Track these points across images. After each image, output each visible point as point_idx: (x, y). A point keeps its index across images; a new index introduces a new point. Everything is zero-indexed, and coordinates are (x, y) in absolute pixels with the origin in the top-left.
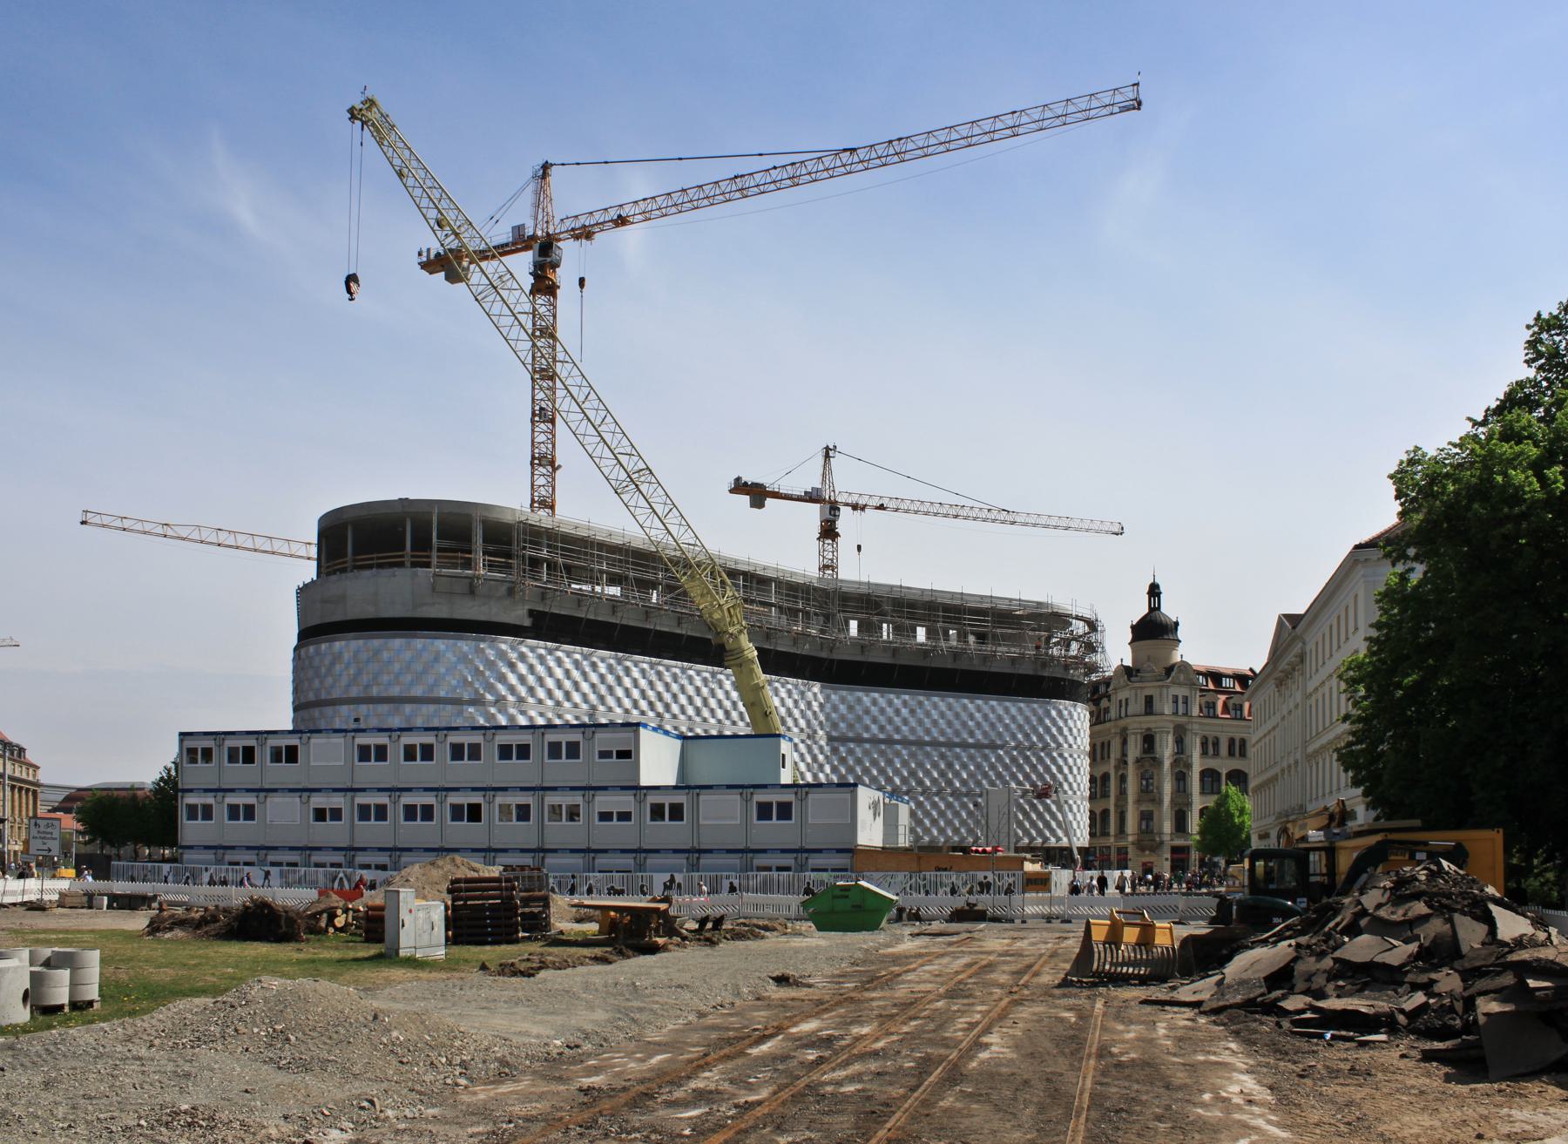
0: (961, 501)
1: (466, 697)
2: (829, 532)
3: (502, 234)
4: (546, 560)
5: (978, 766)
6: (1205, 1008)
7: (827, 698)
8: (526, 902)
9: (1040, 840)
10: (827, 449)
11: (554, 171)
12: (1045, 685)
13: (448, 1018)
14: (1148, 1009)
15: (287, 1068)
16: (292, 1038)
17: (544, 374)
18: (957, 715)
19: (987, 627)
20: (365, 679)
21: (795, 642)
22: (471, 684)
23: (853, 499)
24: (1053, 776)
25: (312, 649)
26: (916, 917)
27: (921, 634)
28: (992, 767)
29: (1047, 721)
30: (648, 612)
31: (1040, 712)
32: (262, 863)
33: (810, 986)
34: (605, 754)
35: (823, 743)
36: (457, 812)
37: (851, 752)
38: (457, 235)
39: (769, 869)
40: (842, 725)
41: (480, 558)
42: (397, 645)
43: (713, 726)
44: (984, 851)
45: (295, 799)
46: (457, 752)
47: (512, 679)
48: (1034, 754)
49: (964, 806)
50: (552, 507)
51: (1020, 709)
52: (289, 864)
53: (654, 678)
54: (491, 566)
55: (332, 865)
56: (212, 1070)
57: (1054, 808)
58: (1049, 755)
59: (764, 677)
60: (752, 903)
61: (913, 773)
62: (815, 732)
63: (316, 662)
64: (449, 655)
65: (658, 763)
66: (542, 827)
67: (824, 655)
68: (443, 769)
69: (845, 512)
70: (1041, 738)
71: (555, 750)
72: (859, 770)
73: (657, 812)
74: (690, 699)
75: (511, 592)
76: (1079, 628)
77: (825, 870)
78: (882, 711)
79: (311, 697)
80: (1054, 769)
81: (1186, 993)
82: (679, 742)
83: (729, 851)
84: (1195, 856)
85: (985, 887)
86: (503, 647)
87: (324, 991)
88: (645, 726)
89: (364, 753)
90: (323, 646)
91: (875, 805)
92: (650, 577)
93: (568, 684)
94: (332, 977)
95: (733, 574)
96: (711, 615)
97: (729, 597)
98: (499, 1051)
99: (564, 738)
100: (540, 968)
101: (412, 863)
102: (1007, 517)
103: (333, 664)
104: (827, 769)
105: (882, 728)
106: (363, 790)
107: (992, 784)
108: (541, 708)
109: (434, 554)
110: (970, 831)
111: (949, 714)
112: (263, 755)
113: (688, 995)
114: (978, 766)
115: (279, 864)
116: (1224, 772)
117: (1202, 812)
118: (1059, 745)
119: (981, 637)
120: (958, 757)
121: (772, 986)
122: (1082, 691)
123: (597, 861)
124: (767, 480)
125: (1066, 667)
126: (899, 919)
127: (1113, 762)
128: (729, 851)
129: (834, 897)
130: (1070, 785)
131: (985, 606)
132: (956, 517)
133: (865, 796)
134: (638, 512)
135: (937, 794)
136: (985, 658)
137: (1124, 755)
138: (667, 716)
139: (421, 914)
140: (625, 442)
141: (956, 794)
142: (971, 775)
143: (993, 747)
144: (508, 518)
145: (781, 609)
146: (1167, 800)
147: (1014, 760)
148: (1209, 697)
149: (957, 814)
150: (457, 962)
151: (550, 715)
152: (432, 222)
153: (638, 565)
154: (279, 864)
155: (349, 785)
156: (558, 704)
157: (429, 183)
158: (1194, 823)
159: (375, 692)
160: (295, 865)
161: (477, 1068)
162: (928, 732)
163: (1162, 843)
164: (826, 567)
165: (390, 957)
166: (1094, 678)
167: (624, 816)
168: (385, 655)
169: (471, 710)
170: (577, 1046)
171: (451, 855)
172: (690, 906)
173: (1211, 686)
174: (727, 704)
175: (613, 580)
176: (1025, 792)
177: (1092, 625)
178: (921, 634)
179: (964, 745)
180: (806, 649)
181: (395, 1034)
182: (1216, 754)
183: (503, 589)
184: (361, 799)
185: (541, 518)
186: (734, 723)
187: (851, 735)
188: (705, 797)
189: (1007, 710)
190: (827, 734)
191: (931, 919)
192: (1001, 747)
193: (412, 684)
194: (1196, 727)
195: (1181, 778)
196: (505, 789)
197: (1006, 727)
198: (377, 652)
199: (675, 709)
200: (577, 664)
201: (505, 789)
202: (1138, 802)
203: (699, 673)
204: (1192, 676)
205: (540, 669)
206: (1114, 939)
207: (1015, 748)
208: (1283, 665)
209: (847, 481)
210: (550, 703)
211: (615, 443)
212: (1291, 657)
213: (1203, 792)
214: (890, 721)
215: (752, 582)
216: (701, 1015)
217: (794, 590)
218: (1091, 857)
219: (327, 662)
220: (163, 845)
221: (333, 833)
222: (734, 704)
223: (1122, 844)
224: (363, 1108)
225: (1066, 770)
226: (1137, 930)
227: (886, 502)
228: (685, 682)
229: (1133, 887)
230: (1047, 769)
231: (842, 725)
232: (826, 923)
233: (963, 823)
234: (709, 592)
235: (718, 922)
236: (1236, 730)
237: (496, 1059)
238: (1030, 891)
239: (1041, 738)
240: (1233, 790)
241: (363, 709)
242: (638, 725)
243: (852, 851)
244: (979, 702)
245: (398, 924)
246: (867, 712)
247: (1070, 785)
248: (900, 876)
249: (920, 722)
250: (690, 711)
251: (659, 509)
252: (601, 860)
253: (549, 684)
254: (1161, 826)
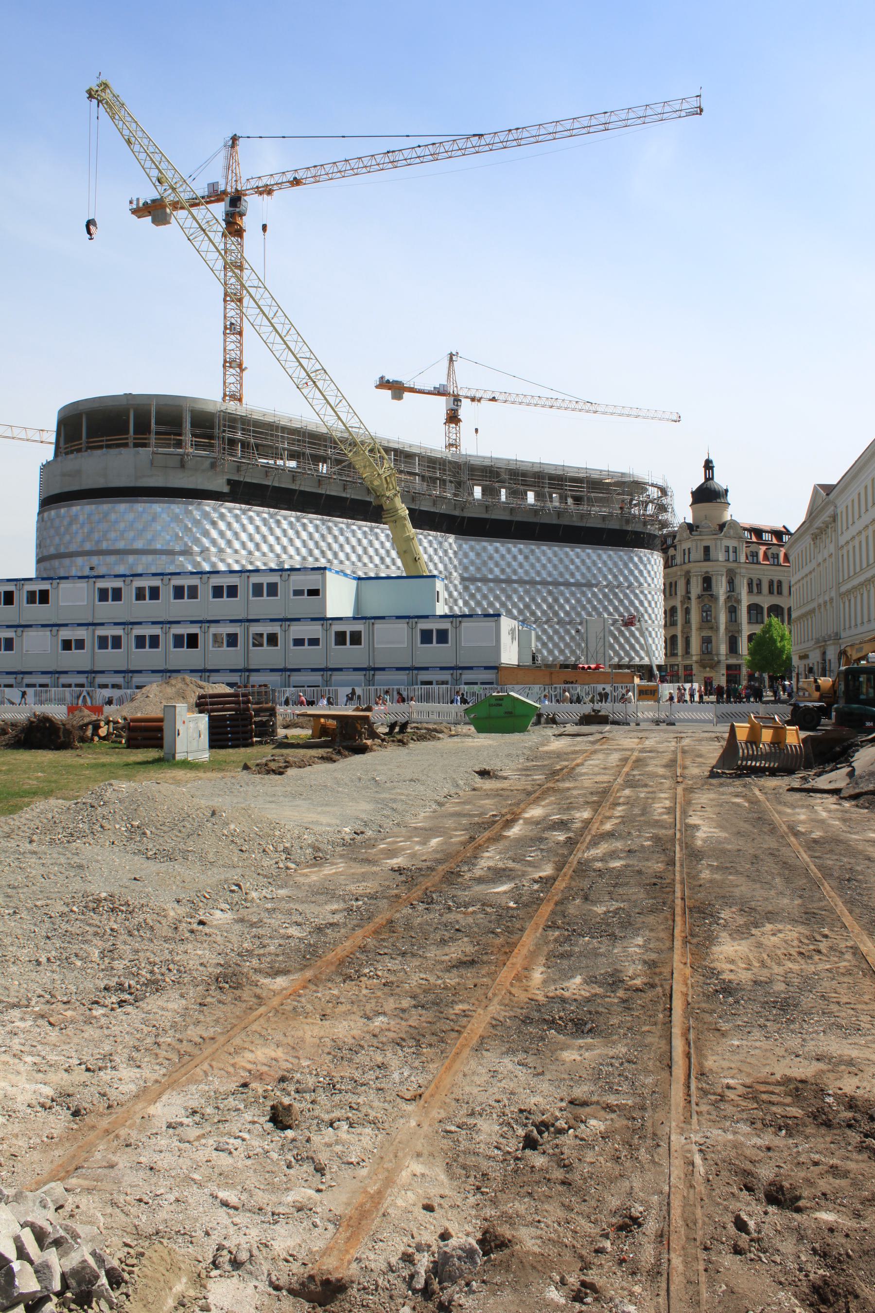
0: (554, 395)
1: (177, 549)
2: (453, 418)
3: (201, 189)
4: (240, 441)
5: (578, 601)
6: (844, 794)
7: (460, 547)
8: (258, 712)
9: (627, 659)
10: (451, 355)
11: (241, 142)
12: (627, 536)
13: (273, 813)
14: (798, 795)
15: (155, 857)
16: (148, 832)
17: (234, 297)
18: (561, 561)
19: (584, 492)
20: (96, 536)
21: (434, 503)
22: (181, 538)
23: (471, 394)
24: (636, 609)
25: (53, 513)
26: (553, 721)
27: (531, 497)
28: (589, 601)
29: (631, 565)
30: (320, 480)
31: (625, 558)
32: (19, 685)
33: (506, 778)
34: (298, 593)
35: (457, 582)
36: (178, 641)
37: (478, 589)
38: (174, 189)
39: (430, 683)
40: (471, 568)
41: (187, 437)
42: (122, 509)
43: (371, 569)
44: (589, 668)
45: (47, 633)
46: (179, 592)
47: (214, 534)
48: (621, 591)
49: (568, 632)
50: (240, 400)
51: (610, 556)
52: (41, 686)
53: (325, 532)
54: (197, 446)
55: (77, 685)
56: (97, 861)
57: (637, 634)
58: (633, 592)
59: (413, 530)
60: (418, 711)
61: (527, 606)
62: (451, 574)
63: (57, 523)
64: (164, 516)
65: (339, 600)
66: (247, 652)
67: (457, 513)
68: (168, 606)
69: (465, 403)
70: (626, 578)
71: (258, 590)
72: (485, 603)
73: (340, 638)
74: (353, 548)
75: (213, 466)
76: (654, 493)
77: (476, 683)
78: (503, 557)
79: (52, 551)
80: (637, 603)
81: (822, 782)
82: (355, 582)
83: (398, 669)
84: (744, 671)
85: (604, 697)
86: (207, 509)
87: (135, 788)
88: (330, 570)
89: (103, 595)
90: (63, 511)
91: (512, 631)
92: (321, 453)
93: (258, 538)
94: (129, 778)
95: (387, 450)
96: (372, 482)
97: (388, 465)
98: (309, 838)
99: (265, 580)
100: (286, 767)
101: (151, 683)
102: (591, 407)
103: (70, 524)
104: (461, 603)
105: (503, 571)
106: (102, 624)
107: (589, 614)
108: (237, 557)
109: (153, 436)
110: (573, 652)
111: (555, 560)
112: (21, 598)
113: (422, 788)
114: (578, 601)
115: (70, 686)
116: (766, 606)
117: (750, 638)
118: (641, 585)
119: (578, 500)
120: (562, 594)
121: (478, 779)
122: (658, 542)
123: (292, 678)
124: (406, 379)
125: (645, 524)
126: (538, 723)
127: (679, 598)
128: (398, 669)
129: (491, 705)
130: (650, 615)
131: (581, 475)
132: (551, 407)
133: (507, 624)
134: (315, 402)
135: (546, 622)
136: (582, 516)
137: (688, 592)
138: (335, 562)
139: (192, 725)
140: (305, 348)
141: (560, 622)
142: (573, 608)
143: (589, 585)
144: (210, 408)
145: (423, 478)
146: (722, 628)
147: (606, 596)
148: (753, 548)
149: (562, 638)
150: (220, 763)
151: (244, 562)
152: (154, 180)
153: (311, 444)
154: (34, 686)
155: (90, 620)
156: (250, 553)
157: (151, 149)
158: (744, 647)
159: (104, 546)
160: (46, 686)
161: (297, 853)
162: (538, 573)
163: (719, 662)
164: (451, 445)
165: (168, 761)
166: (665, 531)
167: (314, 642)
168: (113, 517)
169: (181, 559)
170: (362, 833)
171: (180, 676)
172: (382, 715)
173: (754, 539)
174: (382, 552)
175: (293, 456)
176: (615, 621)
177: (664, 491)
178: (531, 497)
179: (567, 584)
180: (443, 509)
181: (232, 826)
182: (760, 592)
183: (207, 463)
184: (101, 632)
185: (232, 407)
186: (388, 567)
187: (478, 576)
188: (379, 626)
189: (599, 556)
190: (460, 575)
191: (564, 723)
192: (596, 586)
193: (134, 539)
194: (743, 571)
195: (733, 611)
196: (217, 622)
197: (599, 569)
198: (106, 515)
199: (342, 556)
200: (265, 521)
201: (217, 622)
202: (700, 629)
203: (360, 528)
204: (741, 531)
205: (236, 526)
206: (754, 739)
207: (606, 586)
208: (819, 523)
209: (466, 381)
210: (244, 552)
211: (298, 349)
212: (825, 517)
213: (749, 623)
214: (509, 565)
215: (402, 456)
216: (440, 804)
217: (432, 462)
218: (668, 673)
219: (65, 523)
221: (77, 659)
222: (388, 552)
223: (688, 662)
224: (232, 891)
225: (646, 604)
226: (771, 731)
227: (497, 396)
228: (349, 535)
229: (701, 697)
230: (632, 603)
231: (471, 568)
232: (485, 725)
233: (567, 645)
234: (371, 465)
235: (404, 726)
236: (776, 574)
237: (309, 845)
238: (643, 700)
239: (626, 578)
240: (775, 620)
241: (95, 560)
242: (325, 569)
243: (496, 668)
244: (578, 550)
245: (176, 733)
246: (491, 558)
247: (650, 615)
248: (536, 688)
249: (533, 566)
250: (354, 558)
251: (332, 401)
252: (296, 678)
253: (244, 539)
254: (718, 649)
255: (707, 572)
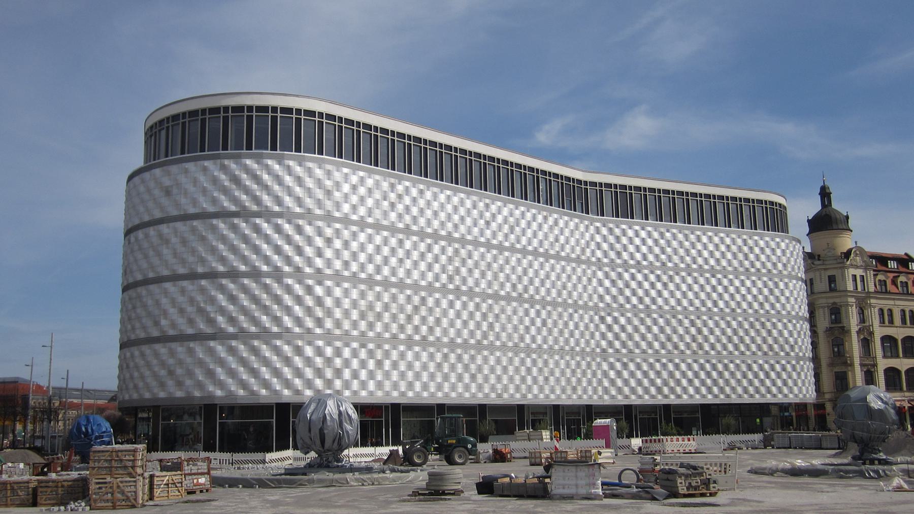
146: (857, 362)
195: (866, 343)
202: (831, 365)
213: (885, 357)
220: (654, 435)
255: (834, 303)
